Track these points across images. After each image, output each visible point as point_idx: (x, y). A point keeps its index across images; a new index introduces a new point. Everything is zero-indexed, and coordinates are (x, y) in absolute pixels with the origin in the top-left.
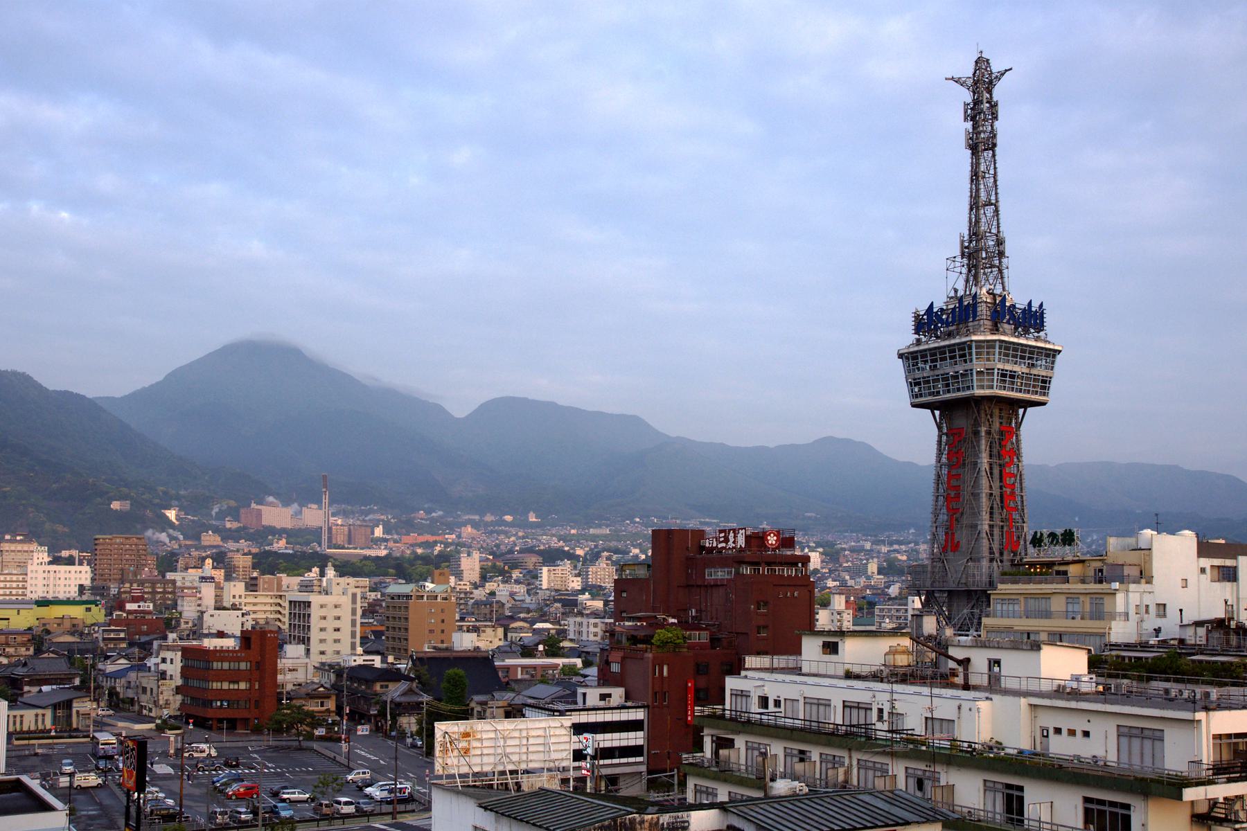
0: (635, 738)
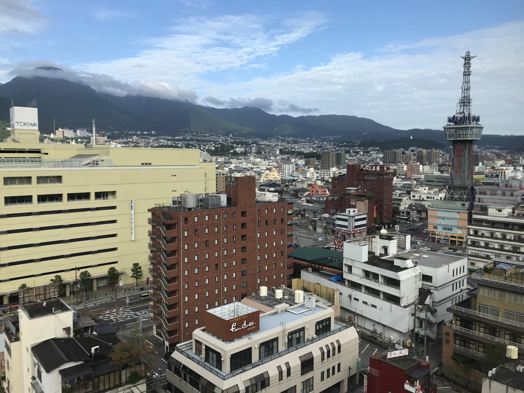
0: (365, 222)
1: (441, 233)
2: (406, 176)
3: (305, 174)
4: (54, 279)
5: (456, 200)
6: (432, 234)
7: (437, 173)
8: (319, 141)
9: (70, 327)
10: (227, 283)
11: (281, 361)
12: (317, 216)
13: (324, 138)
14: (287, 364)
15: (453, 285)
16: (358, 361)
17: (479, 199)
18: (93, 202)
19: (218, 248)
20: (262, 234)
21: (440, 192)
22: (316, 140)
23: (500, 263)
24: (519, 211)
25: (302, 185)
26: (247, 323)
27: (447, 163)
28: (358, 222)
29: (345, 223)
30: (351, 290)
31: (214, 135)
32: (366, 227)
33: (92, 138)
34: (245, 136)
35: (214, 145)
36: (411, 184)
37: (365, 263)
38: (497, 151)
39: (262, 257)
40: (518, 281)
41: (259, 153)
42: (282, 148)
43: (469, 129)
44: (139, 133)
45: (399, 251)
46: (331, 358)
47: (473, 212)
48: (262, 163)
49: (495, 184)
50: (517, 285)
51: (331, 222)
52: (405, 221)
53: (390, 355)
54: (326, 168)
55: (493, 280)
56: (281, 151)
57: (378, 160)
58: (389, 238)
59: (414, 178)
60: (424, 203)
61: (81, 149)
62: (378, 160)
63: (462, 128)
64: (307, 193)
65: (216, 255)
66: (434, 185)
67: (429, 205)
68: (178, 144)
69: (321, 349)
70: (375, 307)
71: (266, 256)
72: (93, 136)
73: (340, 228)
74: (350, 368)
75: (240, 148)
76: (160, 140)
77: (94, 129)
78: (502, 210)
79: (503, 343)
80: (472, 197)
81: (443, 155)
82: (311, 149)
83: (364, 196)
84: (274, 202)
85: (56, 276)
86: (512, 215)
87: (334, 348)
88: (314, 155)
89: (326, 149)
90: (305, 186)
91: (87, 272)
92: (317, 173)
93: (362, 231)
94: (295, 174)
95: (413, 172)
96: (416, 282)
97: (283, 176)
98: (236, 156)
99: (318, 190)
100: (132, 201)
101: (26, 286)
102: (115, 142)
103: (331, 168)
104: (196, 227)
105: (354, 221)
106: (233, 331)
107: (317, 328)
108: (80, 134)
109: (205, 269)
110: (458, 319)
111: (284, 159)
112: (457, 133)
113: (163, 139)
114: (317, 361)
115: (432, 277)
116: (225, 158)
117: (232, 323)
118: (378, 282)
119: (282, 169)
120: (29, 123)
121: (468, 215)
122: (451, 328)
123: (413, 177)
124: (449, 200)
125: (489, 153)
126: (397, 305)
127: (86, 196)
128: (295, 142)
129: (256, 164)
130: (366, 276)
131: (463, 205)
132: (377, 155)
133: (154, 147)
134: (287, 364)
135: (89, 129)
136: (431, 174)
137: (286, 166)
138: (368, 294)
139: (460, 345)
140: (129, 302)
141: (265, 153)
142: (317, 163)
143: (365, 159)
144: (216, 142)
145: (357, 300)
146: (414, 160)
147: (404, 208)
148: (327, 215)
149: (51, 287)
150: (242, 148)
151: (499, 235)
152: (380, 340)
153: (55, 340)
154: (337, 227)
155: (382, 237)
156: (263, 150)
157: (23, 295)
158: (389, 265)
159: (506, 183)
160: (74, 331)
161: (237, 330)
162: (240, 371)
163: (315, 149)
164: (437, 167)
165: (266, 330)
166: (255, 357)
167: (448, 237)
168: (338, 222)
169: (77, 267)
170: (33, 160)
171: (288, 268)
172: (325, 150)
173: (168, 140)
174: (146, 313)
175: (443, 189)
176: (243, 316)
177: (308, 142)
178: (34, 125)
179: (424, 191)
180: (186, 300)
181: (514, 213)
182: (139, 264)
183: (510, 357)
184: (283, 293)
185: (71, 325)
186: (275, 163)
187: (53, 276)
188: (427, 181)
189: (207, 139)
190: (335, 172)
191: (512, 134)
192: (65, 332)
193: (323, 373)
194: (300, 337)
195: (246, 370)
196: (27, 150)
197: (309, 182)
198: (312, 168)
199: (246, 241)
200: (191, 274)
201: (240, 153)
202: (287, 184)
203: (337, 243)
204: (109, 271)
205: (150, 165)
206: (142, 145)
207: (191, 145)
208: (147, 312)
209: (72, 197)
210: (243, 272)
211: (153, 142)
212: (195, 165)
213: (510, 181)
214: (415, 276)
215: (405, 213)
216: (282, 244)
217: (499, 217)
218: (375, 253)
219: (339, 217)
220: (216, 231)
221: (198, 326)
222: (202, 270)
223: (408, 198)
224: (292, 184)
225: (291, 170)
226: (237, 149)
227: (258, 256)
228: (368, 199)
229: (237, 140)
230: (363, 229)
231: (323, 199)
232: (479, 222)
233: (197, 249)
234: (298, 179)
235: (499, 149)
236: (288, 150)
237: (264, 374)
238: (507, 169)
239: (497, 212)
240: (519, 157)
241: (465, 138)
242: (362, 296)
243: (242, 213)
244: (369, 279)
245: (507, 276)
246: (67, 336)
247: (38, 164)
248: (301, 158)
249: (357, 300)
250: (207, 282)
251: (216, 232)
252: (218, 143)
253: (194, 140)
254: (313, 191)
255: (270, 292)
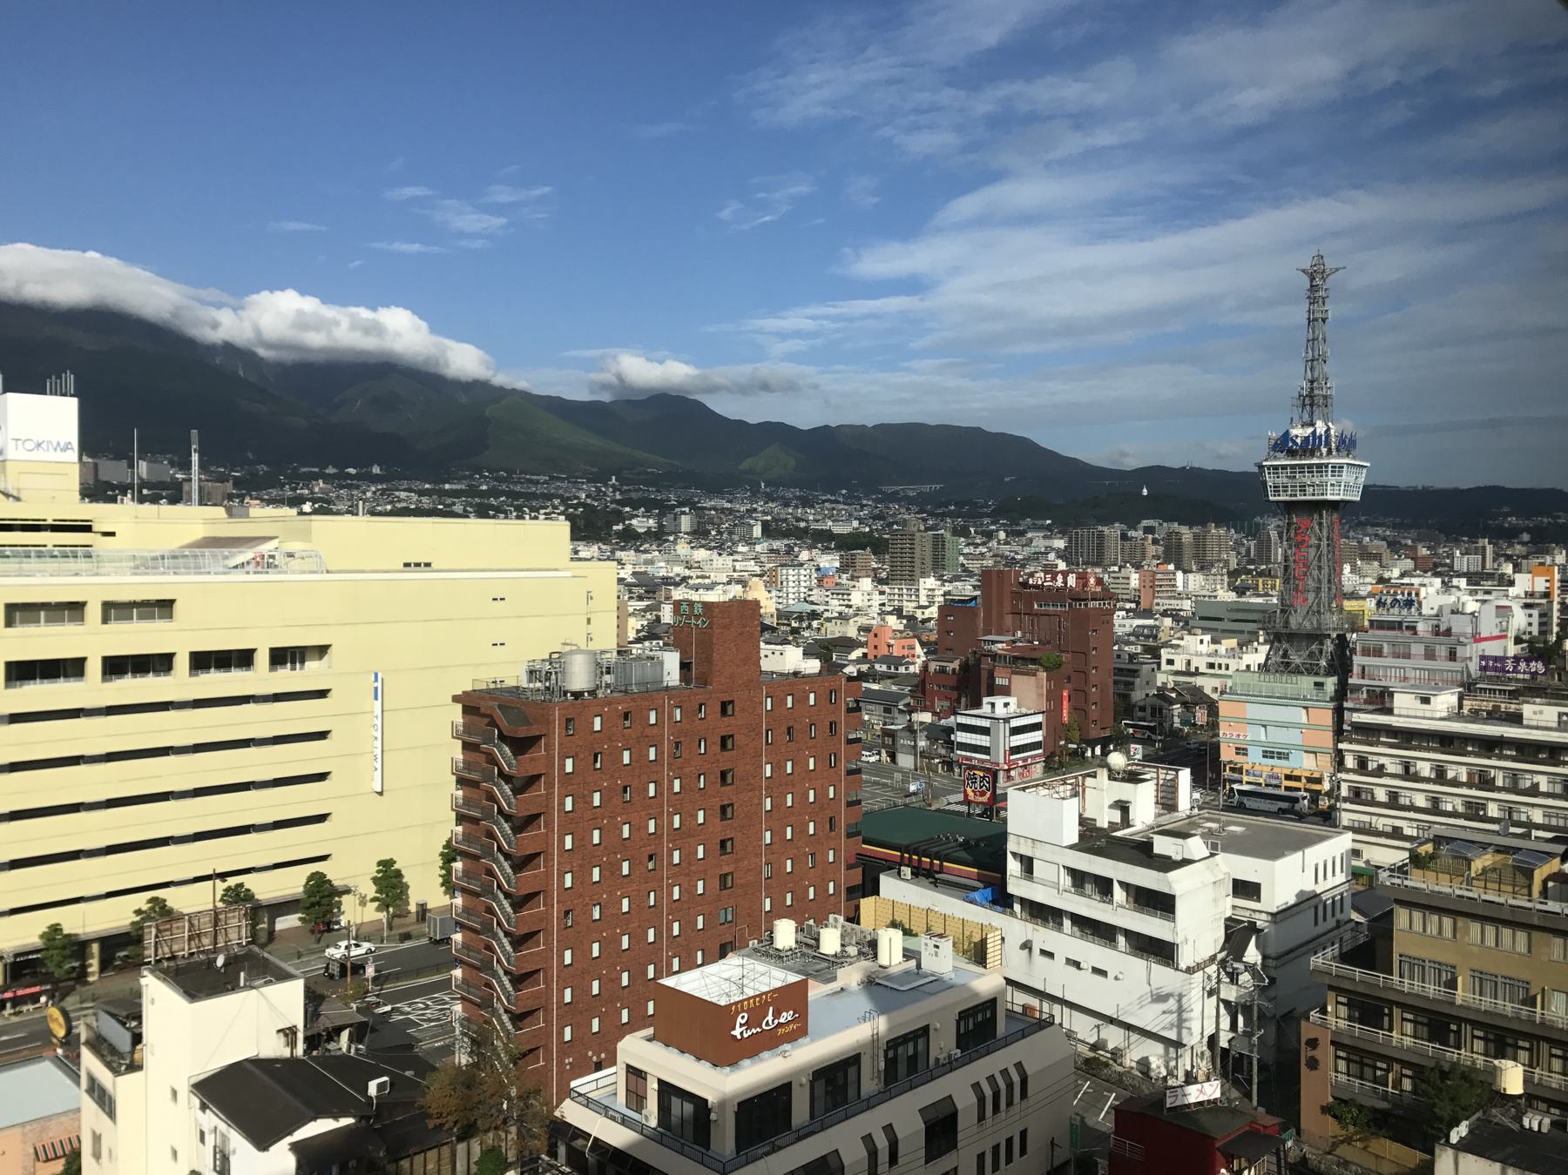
0: (1037, 736)
1: (1257, 767)
2: (1138, 603)
3: (845, 597)
4: (145, 907)
5: (1297, 671)
6: (1233, 770)
7: (1226, 596)
8: (877, 501)
9: (295, 1027)
10: (682, 910)
11: (871, 1122)
12: (893, 718)
13: (890, 489)
14: (889, 1129)
15: (1316, 908)
16: (1072, 1125)
17: (1364, 667)
18: (261, 680)
19: (654, 808)
20: (778, 767)
21: (1241, 649)
22: (867, 496)
24: (1474, 703)
25: (842, 629)
26: (777, 1015)
27: (1253, 567)
28: (1018, 737)
29: (982, 740)
30: (1030, 926)
31: (562, 480)
32: (1040, 751)
33: (186, 487)
34: (654, 481)
35: (562, 508)
36: (1157, 627)
37: (1072, 847)
38: (1388, 533)
39: (778, 834)
40: (1503, 887)
41: (699, 535)
42: (769, 518)
43: (1330, 469)
44: (331, 470)
45: (1160, 815)
46: (1002, 1115)
47: (1346, 705)
48: (715, 563)
49: (1405, 624)
50: (1501, 900)
51: (942, 735)
52: (1148, 733)
53: (1173, 1099)
54: (904, 577)
55: (1437, 888)
56: (765, 525)
57: (1052, 556)
58: (1132, 777)
59: (1162, 609)
60: (1199, 681)
61: (213, 521)
62: (1052, 556)
63: (1310, 466)
64: (857, 653)
65: (652, 829)
66: (1223, 631)
67: (1216, 688)
68: (454, 504)
69: (976, 1087)
70: (1103, 973)
71: (789, 830)
72: (190, 480)
73: (969, 754)
74: (1052, 1142)
75: (643, 517)
76: (397, 493)
77: (195, 458)
78: (1432, 698)
79: (1469, 1063)
80: (1341, 665)
81: (1238, 543)
82: (855, 524)
83: (1034, 661)
84: (809, 676)
85: (150, 901)
86: (1458, 716)
87: (1010, 1086)
88: (865, 540)
89: (897, 523)
90: (852, 632)
91: (241, 885)
92: (882, 593)
93: (1029, 761)
94: (817, 595)
95: (1158, 592)
96: (1216, 901)
97: (780, 600)
98: (633, 542)
99: (892, 642)
100: (376, 675)
101: (61, 930)
102: (256, 499)
103: (922, 580)
104: (596, 746)
105: (1007, 734)
106: (739, 1037)
107: (962, 1031)
108: (148, 473)
109: (621, 869)
110: (1340, 999)
111: (776, 552)
113: (404, 490)
114: (966, 1121)
115: (1260, 884)
116: (599, 549)
117: (737, 1013)
118: (1111, 902)
119: (777, 580)
120: (50, 442)
121: (1333, 714)
122: (1324, 1026)
123: (1157, 607)
124: (1277, 671)
125: (1368, 539)
126: (1168, 965)
127: (244, 659)
128: (806, 503)
129: (697, 565)
130: (1074, 885)
131: (1319, 685)
132: (1048, 543)
133: (380, 514)
134: (889, 1129)
135: (176, 459)
136: (1210, 597)
137: (791, 572)
138: (1081, 938)
139: (1349, 1075)
140: (373, 974)
141: (720, 533)
142: (875, 565)
143: (1012, 554)
144: (569, 499)
145: (1050, 955)
146: (1156, 557)
147: (1144, 696)
148: (926, 717)
149: (231, 915)
150: (648, 517)
151: (1425, 769)
152: (1119, 1069)
153: (257, 1062)
154: (959, 752)
155: (1113, 776)
156: (713, 524)
157: (157, 937)
158: (1142, 852)
159: (1435, 622)
160: (306, 1039)
161: (749, 1033)
162: (760, 1151)
163: (866, 522)
164: (1226, 578)
165: (824, 1034)
166: (800, 1110)
167: (1278, 778)
168: (961, 737)
169: (217, 872)
170: (68, 553)
171: (849, 867)
172: (895, 527)
173: (421, 493)
174: (427, 1007)
175: (1250, 642)
176: (760, 996)
177: (845, 504)
178: (67, 447)
179: (1196, 648)
180: (568, 960)
181: (1460, 706)
182: (395, 862)
183: (1505, 1089)
184: (843, 937)
185: (298, 1020)
186: (752, 562)
187: (303, 873)
188: (1202, 618)
189: (540, 490)
190: (934, 590)
191: (1428, 483)
192: (282, 1039)
193: (981, 1157)
194: (916, 1053)
195: (780, 1148)
196: (50, 522)
197: (862, 621)
198: (865, 579)
199: (734, 787)
200: (582, 883)
201: (645, 533)
202: (794, 624)
203: (971, 794)
204: (307, 883)
205: (427, 569)
206: (341, 507)
207: (492, 507)
208: (429, 1003)
209: (202, 661)
210: (723, 877)
211: (375, 500)
212: (558, 567)
213: (1446, 616)
214: (1215, 883)
215: (1149, 710)
216: (831, 796)
217: (1424, 718)
218: (1095, 820)
219: (964, 722)
220: (652, 757)
221: (631, 1027)
222: (611, 870)
223: (1155, 666)
224: (809, 627)
225: (803, 584)
226: (634, 522)
227: (766, 830)
228: (1047, 669)
229: (634, 495)
230: (1033, 757)
231: (907, 669)
232: (1369, 733)
233: (598, 810)
234: (828, 610)
235: (1394, 527)
236: (788, 525)
237: (829, 1158)
238: (1424, 585)
239: (1418, 704)
240: (1451, 550)
242: (1066, 942)
243: (724, 706)
244: (1083, 895)
245: (1473, 875)
246: (286, 1053)
247: (82, 564)
248: (826, 550)
249: (1050, 955)
250: (625, 908)
251: (651, 761)
252: (575, 502)
253: (502, 493)
254: (876, 647)
255: (801, 938)
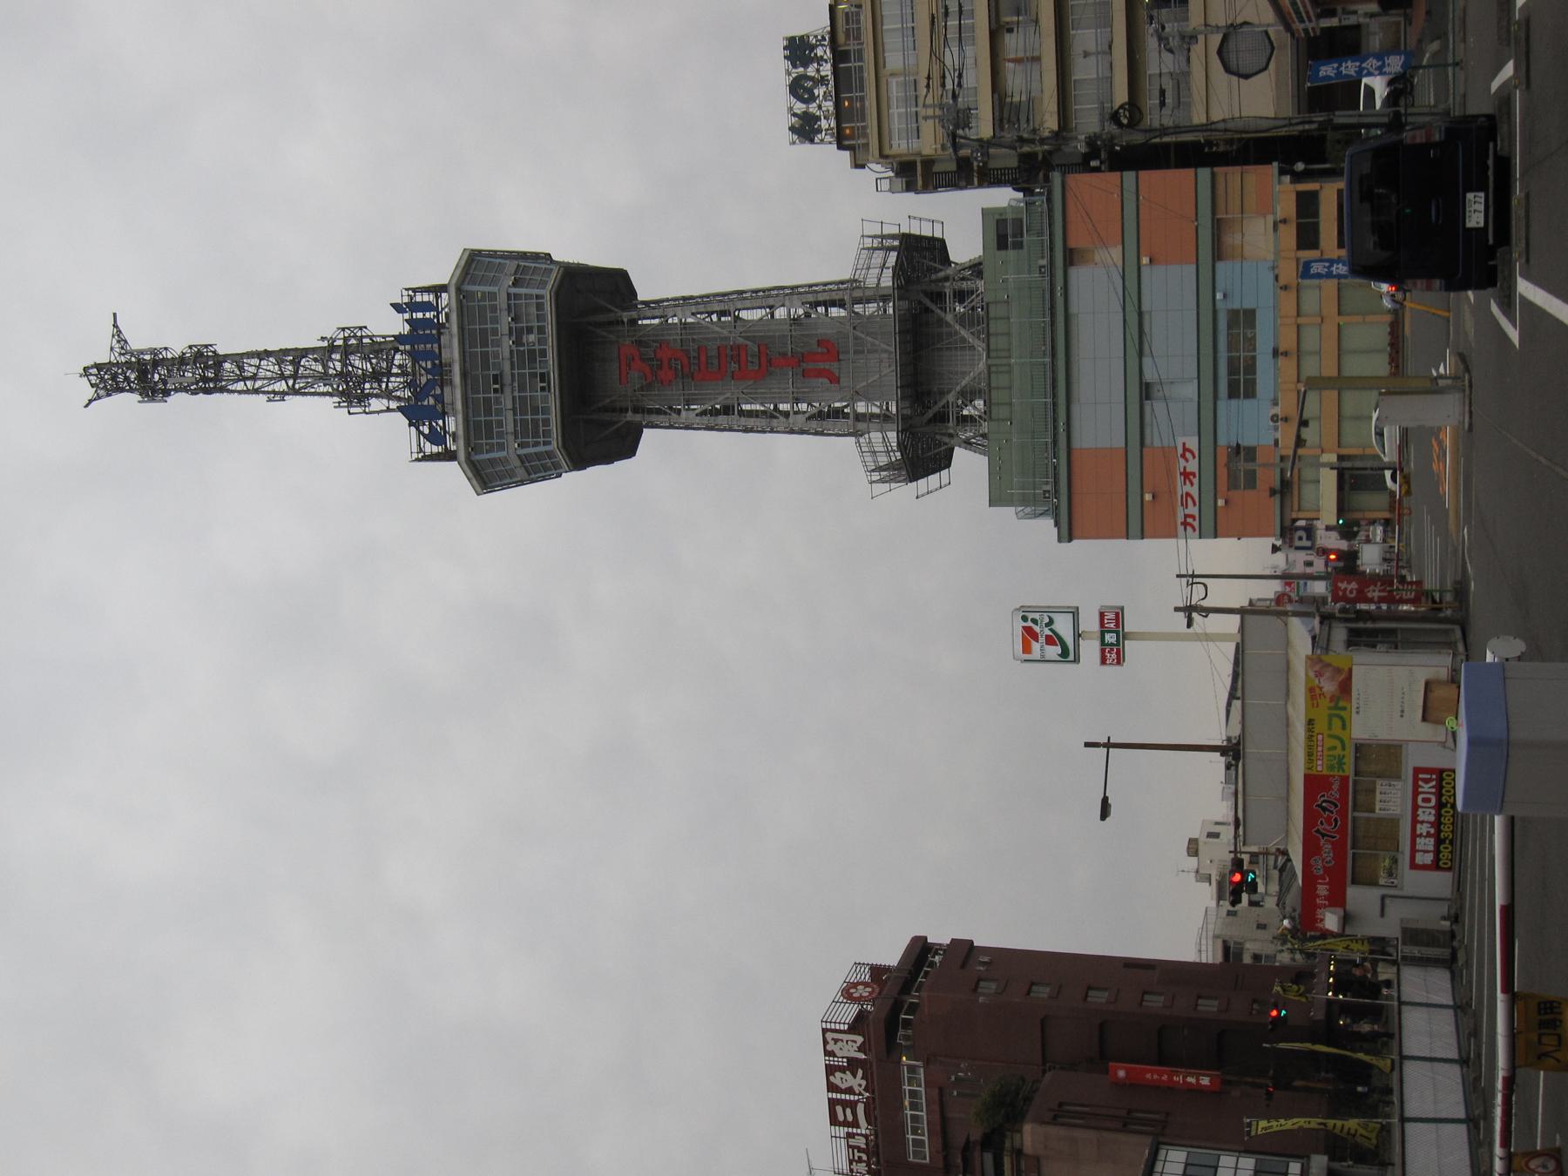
23: (1274, 607)
112: (507, 379)
241: (540, 318)
